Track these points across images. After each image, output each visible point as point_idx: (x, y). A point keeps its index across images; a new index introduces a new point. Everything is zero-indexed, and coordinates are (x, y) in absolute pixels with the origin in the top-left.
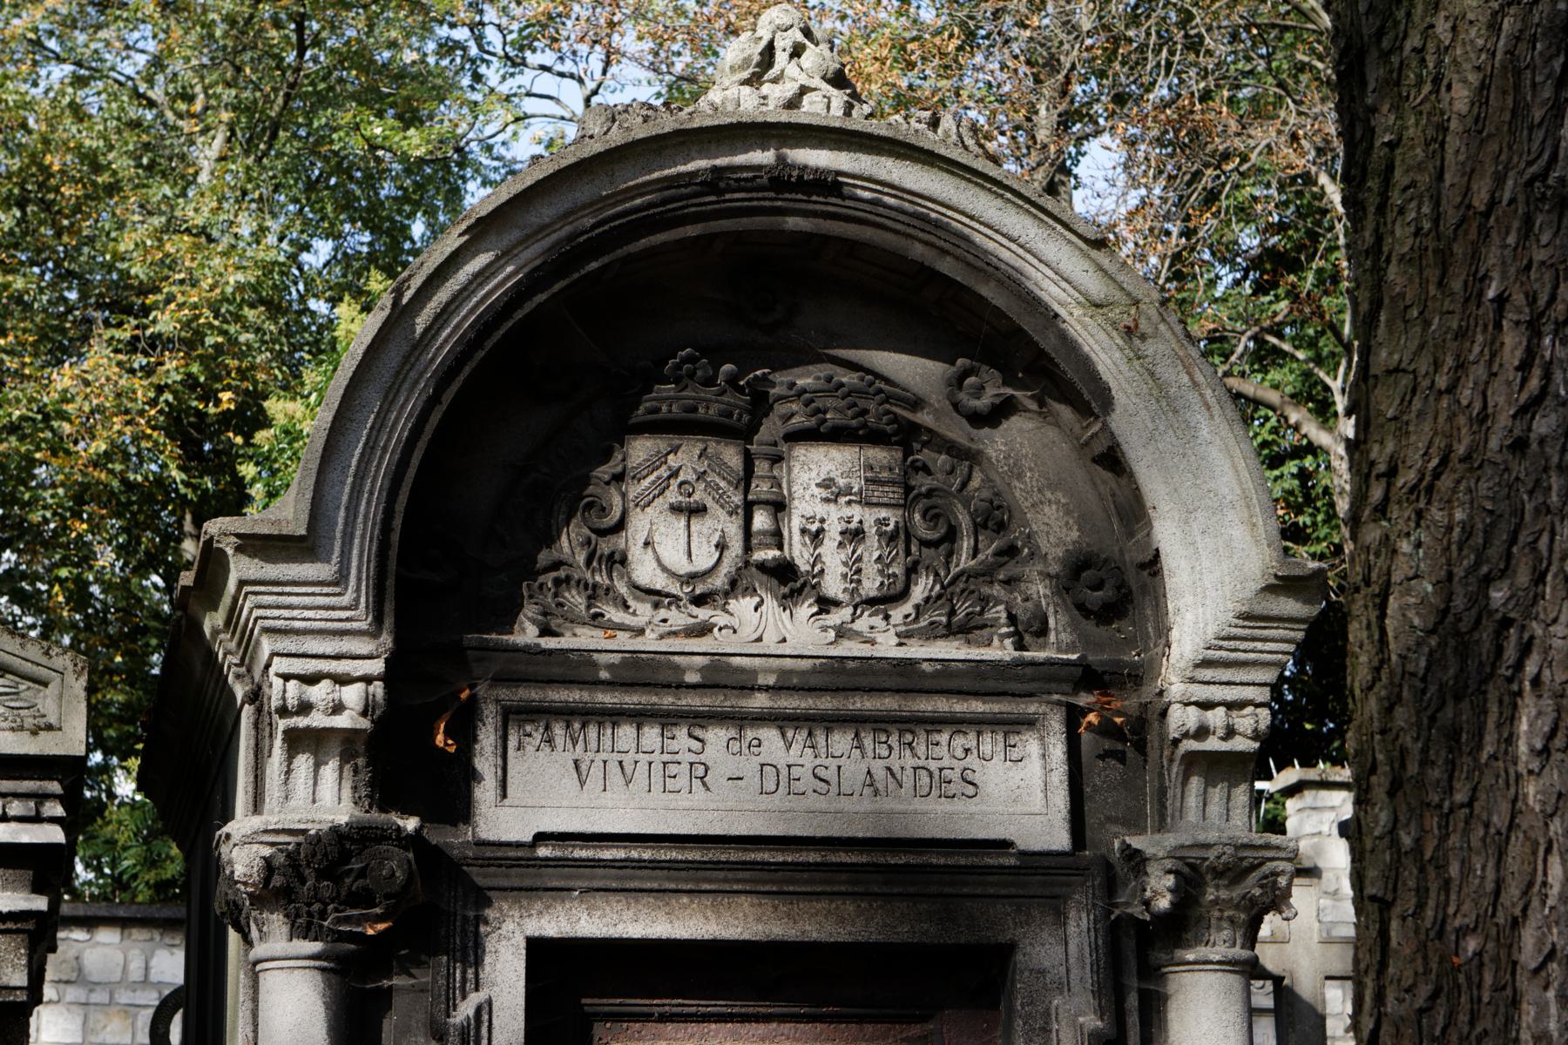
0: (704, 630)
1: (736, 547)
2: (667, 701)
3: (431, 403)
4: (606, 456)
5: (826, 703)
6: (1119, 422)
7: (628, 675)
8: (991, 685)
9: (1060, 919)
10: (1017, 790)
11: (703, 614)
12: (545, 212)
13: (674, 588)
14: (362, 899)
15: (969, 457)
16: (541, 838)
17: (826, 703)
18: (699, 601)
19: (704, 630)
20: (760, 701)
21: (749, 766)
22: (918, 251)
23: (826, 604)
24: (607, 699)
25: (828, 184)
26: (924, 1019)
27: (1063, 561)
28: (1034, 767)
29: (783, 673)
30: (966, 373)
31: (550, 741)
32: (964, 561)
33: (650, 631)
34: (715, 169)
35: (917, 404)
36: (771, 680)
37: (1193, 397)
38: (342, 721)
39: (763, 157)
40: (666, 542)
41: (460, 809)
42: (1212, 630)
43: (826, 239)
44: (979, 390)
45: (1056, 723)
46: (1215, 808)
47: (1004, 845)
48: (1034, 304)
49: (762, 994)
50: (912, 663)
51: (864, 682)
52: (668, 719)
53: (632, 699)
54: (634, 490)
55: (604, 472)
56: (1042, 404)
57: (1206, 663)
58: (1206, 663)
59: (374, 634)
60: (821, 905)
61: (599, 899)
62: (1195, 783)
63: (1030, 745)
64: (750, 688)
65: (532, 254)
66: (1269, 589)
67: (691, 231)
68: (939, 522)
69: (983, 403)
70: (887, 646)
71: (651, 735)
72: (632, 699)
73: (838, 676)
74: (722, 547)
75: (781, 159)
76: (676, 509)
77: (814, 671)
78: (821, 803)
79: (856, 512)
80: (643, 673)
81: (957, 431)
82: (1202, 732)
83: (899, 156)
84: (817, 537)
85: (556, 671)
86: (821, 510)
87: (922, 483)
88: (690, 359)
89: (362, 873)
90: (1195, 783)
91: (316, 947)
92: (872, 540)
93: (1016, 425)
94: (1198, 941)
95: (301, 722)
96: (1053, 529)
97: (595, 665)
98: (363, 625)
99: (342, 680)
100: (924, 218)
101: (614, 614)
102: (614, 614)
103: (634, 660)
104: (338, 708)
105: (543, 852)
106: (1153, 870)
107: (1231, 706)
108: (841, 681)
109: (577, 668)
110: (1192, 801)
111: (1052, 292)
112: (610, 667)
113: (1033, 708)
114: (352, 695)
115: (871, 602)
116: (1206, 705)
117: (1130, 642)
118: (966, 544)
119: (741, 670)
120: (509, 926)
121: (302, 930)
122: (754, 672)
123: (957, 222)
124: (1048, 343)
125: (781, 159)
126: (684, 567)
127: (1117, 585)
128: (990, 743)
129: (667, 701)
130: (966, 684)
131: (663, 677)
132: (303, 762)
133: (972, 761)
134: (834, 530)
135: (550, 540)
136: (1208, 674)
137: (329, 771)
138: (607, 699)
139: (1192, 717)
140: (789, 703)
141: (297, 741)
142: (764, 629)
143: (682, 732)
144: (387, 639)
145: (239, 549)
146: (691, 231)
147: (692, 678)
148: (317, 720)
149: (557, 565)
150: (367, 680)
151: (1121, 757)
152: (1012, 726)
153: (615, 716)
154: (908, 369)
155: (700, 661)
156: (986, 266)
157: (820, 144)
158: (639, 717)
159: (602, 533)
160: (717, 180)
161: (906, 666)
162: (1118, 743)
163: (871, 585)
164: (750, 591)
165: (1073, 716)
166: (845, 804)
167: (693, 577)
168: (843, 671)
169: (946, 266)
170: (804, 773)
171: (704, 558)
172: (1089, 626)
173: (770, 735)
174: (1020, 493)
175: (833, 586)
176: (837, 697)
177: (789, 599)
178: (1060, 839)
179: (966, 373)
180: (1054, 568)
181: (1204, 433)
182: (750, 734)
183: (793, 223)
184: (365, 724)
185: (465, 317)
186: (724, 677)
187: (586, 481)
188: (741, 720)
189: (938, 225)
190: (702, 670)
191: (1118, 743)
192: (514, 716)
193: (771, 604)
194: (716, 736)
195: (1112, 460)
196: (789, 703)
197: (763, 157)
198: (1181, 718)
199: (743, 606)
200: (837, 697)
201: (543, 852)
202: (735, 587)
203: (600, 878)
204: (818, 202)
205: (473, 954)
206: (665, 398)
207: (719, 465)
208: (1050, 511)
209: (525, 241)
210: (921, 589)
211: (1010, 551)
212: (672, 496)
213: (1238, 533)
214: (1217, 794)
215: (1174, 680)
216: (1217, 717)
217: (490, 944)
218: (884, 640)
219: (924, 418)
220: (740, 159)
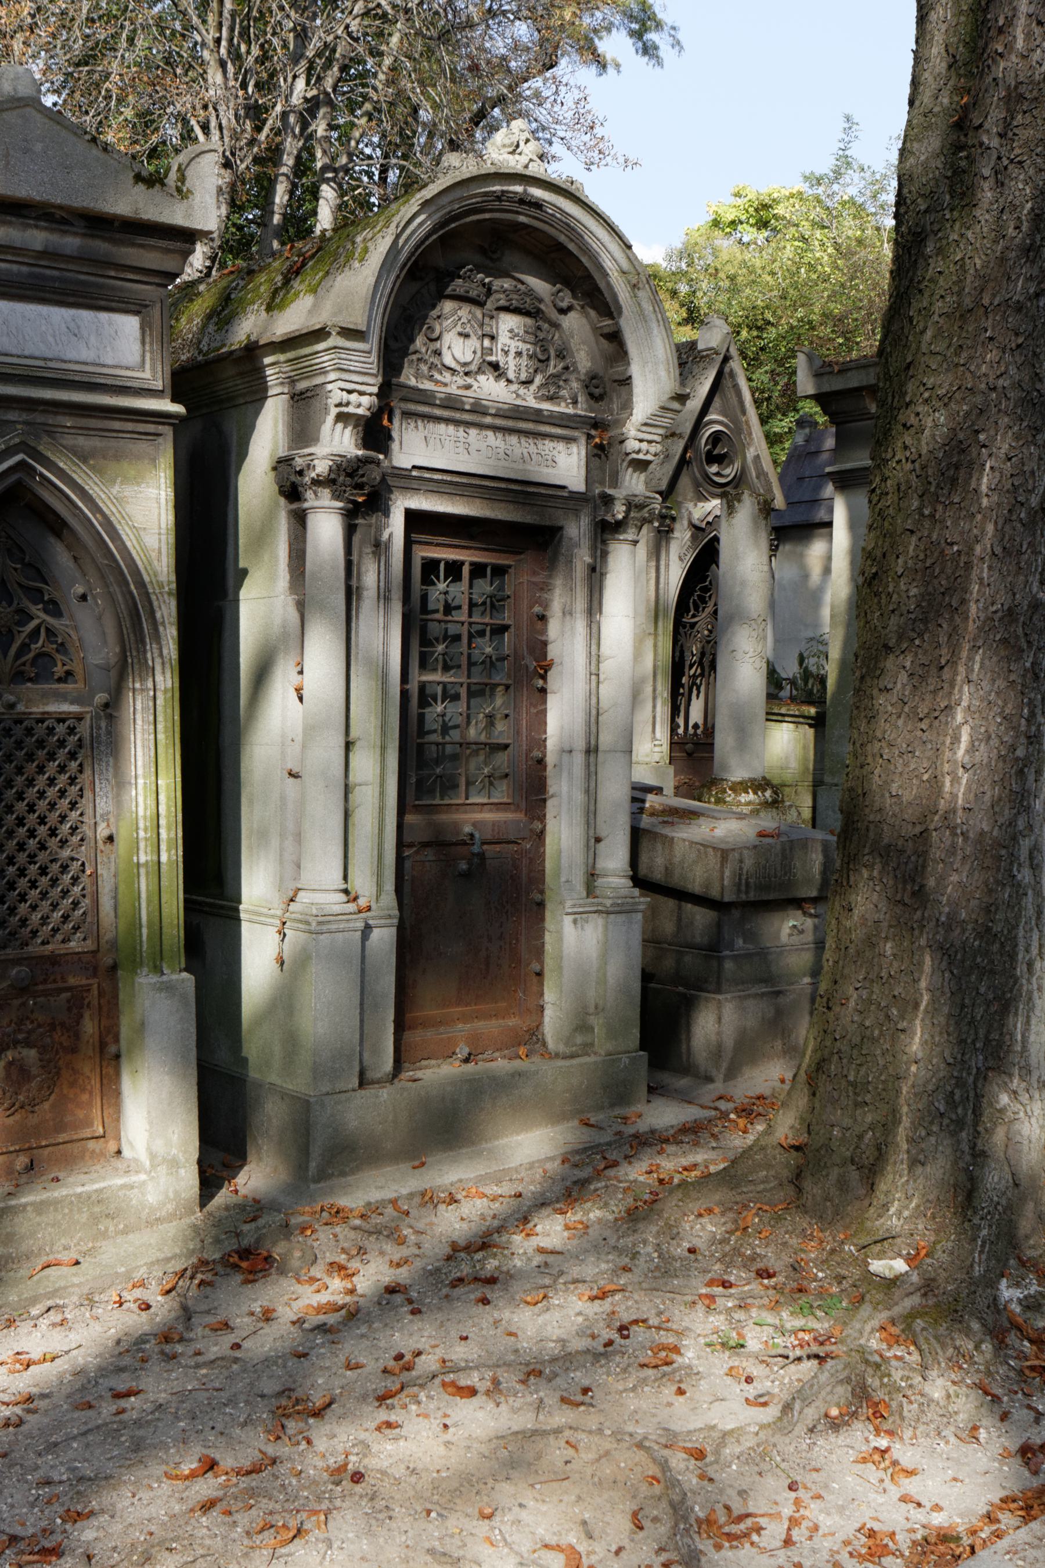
0: (468, 387)
1: (479, 354)
2: (457, 415)
3: (398, 277)
4: (434, 307)
5: (510, 423)
6: (623, 322)
7: (446, 404)
8: (564, 423)
9: (578, 517)
10: (566, 465)
11: (469, 380)
12: (445, 200)
13: (458, 368)
14: (359, 486)
15: (556, 326)
16: (414, 467)
17: (510, 423)
18: (466, 374)
19: (468, 387)
20: (488, 420)
21: (483, 446)
22: (562, 238)
23: (509, 381)
24: (438, 412)
25: (537, 205)
26: (521, 553)
27: (587, 374)
28: (575, 457)
29: (499, 409)
30: (559, 291)
31: (416, 427)
32: (552, 370)
33: (453, 385)
34: (503, 192)
35: (541, 301)
36: (493, 411)
37: (653, 316)
38: (360, 411)
39: (519, 189)
40: (457, 349)
41: (386, 451)
42: (650, 412)
43: (536, 229)
44: (562, 300)
45: (583, 440)
46: (634, 481)
47: (563, 487)
48: (600, 268)
49: (471, 538)
50: (541, 410)
51: (524, 416)
52: (457, 423)
53: (446, 413)
54: (446, 323)
55: (434, 313)
56: (582, 307)
57: (646, 424)
58: (646, 424)
59: (376, 376)
60: (503, 505)
61: (429, 495)
62: (630, 470)
63: (574, 448)
64: (485, 414)
65: (437, 217)
66: (672, 398)
67: (487, 216)
68: (547, 351)
69: (564, 305)
70: (532, 403)
71: (451, 428)
72: (446, 413)
73: (517, 413)
74: (474, 352)
75: (525, 191)
76: (460, 334)
77: (509, 410)
78: (506, 464)
79: (520, 344)
80: (452, 403)
81: (554, 315)
82: (639, 452)
83: (566, 197)
84: (506, 353)
85: (422, 398)
86: (508, 342)
87: (541, 335)
88: (471, 270)
89: (363, 476)
90: (630, 470)
91: (340, 504)
92: (525, 357)
93: (572, 315)
94: (625, 532)
95: (345, 410)
96: (584, 360)
97: (463, 403)
98: (375, 371)
99: (361, 393)
100: (568, 225)
101: (437, 376)
102: (437, 376)
103: (450, 397)
104: (359, 406)
105: (414, 473)
106: (617, 502)
107: (650, 442)
108: (517, 415)
109: (425, 398)
110: (628, 478)
111: (608, 264)
112: (441, 399)
113: (576, 434)
114: (365, 400)
115: (523, 383)
116: (641, 441)
117: (604, 411)
118: (552, 363)
119: (485, 406)
120: (399, 503)
121: (336, 497)
122: (487, 407)
123: (580, 228)
124: (602, 285)
125: (525, 191)
126: (462, 360)
127: (608, 386)
128: (561, 446)
129: (457, 415)
130: (557, 422)
131: (458, 406)
132: (340, 426)
133: (555, 452)
134: (513, 351)
135: (412, 340)
136: (644, 428)
137: (348, 430)
138: (438, 412)
139: (636, 445)
140: (499, 422)
141: (341, 417)
142: (490, 390)
143: (461, 429)
144: (380, 379)
145: (338, 333)
146: (487, 216)
147: (467, 407)
148: (351, 409)
149: (416, 352)
150: (370, 395)
151: (600, 457)
152: (569, 440)
153: (438, 419)
154: (538, 285)
155: (472, 400)
156: (587, 250)
157: (539, 187)
158: (447, 421)
159: (431, 340)
160: (500, 197)
161: (539, 411)
162: (604, 451)
163: (523, 376)
164: (484, 373)
165: (589, 437)
166: (514, 465)
167: (465, 364)
168: (518, 411)
169: (571, 247)
170: (501, 451)
171: (468, 358)
172: (592, 402)
173: (490, 433)
174: (574, 343)
175: (511, 375)
176: (516, 422)
177: (498, 378)
178: (582, 488)
179: (559, 291)
180: (583, 377)
181: (655, 332)
182: (484, 433)
183: (522, 219)
184: (368, 413)
185: (412, 242)
186: (478, 408)
187: (426, 317)
188: (481, 426)
189: (573, 229)
190: (472, 404)
191: (604, 451)
192: (407, 415)
193: (492, 379)
194: (473, 432)
195: (615, 337)
196: (499, 422)
197: (519, 189)
198: (632, 445)
199: (482, 378)
200: (516, 422)
201: (414, 473)
202: (480, 371)
203: (432, 486)
204: (533, 212)
205: (387, 513)
206: (458, 286)
207: (474, 316)
208: (582, 353)
209: (438, 210)
210: (538, 380)
211: (566, 368)
212: (459, 329)
213: (663, 373)
214: (636, 475)
215: (631, 429)
216: (354, 397)
217: (392, 509)
218: (530, 399)
219: (542, 307)
220: (512, 188)
